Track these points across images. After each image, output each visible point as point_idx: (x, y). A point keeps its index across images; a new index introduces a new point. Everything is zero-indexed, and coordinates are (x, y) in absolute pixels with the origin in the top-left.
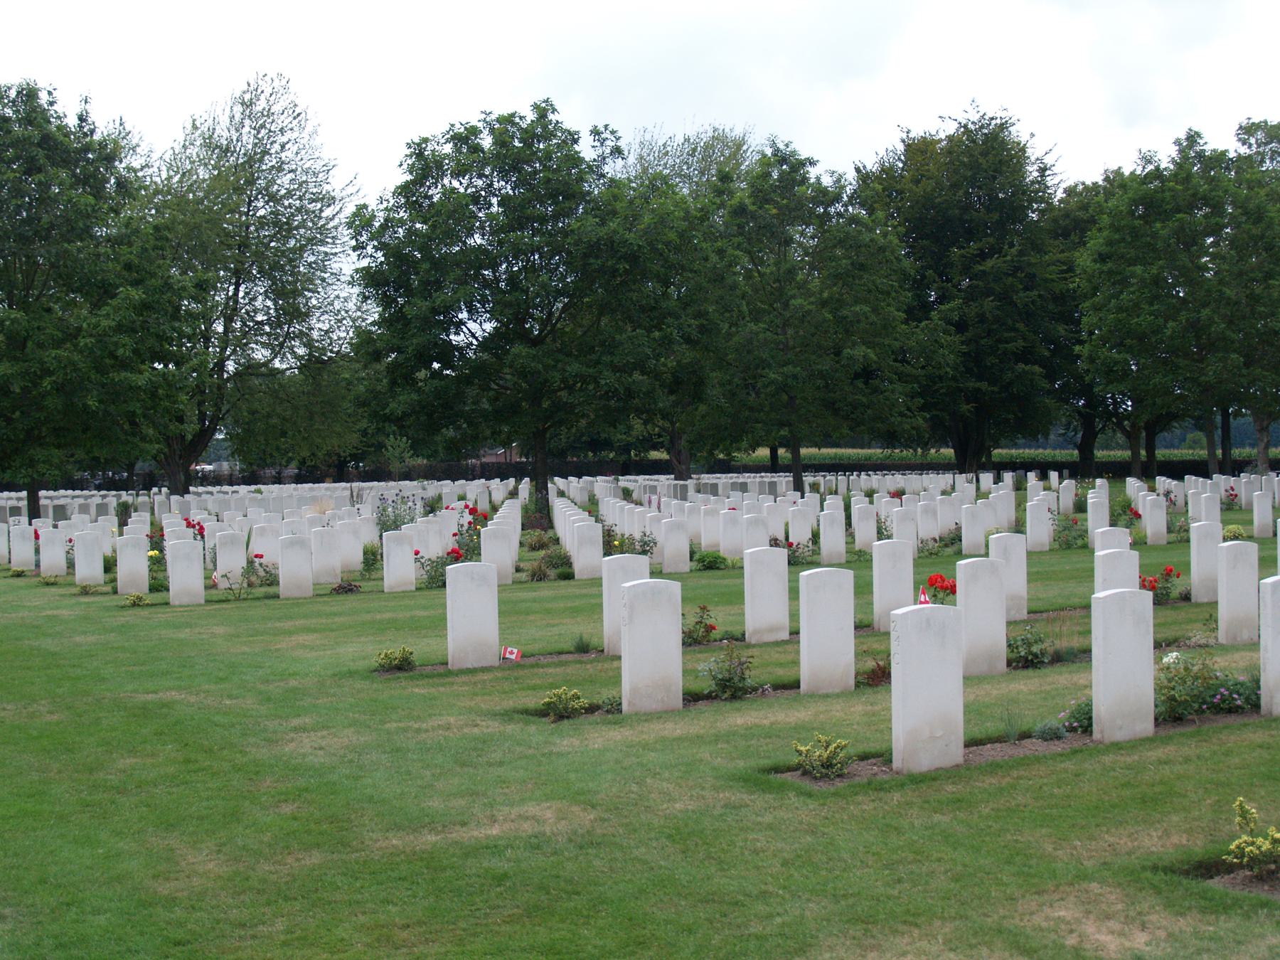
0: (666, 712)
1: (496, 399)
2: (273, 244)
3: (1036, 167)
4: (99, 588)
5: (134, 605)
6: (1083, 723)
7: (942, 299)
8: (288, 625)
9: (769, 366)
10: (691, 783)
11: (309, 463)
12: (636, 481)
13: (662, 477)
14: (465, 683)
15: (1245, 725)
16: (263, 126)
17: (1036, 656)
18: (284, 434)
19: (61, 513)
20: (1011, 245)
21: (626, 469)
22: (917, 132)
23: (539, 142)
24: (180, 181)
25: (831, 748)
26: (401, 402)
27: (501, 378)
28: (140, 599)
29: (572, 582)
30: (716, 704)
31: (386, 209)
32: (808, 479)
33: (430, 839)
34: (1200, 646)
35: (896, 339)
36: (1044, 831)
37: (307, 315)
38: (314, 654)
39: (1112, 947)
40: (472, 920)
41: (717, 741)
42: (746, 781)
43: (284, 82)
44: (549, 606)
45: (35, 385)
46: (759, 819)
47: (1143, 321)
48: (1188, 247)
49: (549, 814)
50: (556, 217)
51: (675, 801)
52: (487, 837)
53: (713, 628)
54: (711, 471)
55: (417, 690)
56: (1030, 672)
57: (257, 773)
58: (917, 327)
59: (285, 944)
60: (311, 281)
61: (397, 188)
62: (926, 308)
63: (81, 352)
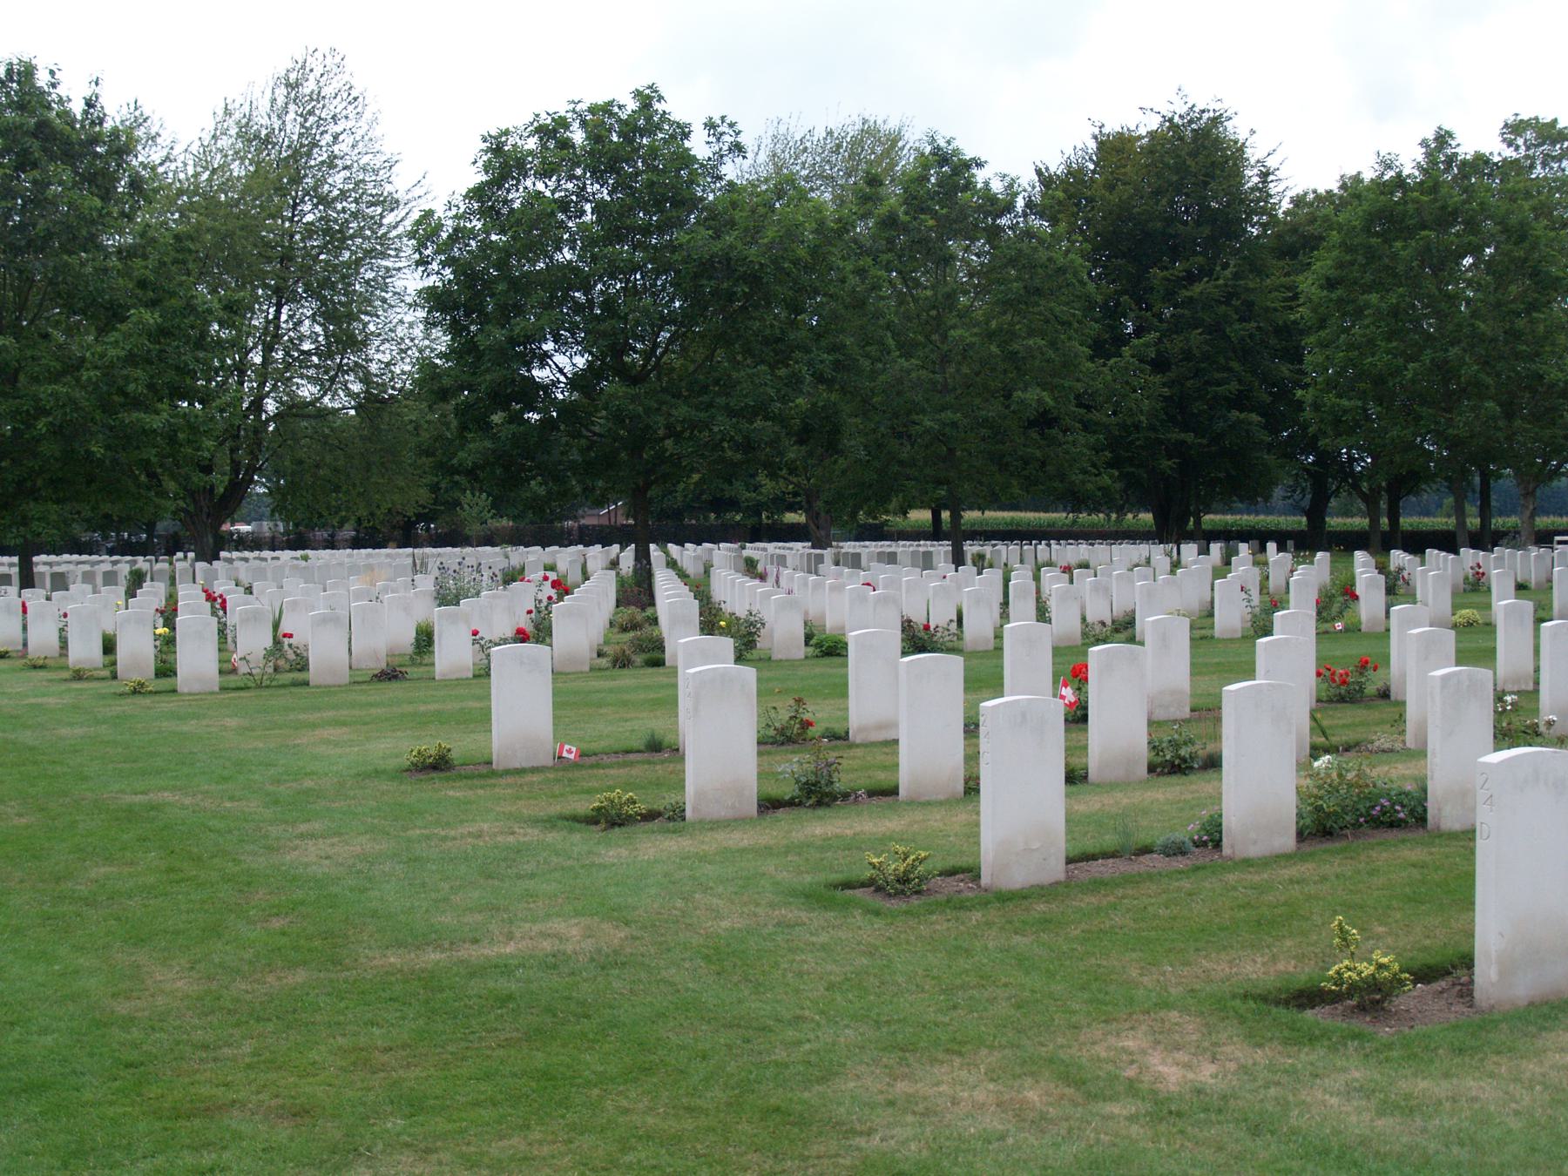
0: (735, 820)
1: (589, 448)
2: (322, 257)
3: (1256, 171)
4: (95, 673)
5: (135, 692)
6: (1212, 838)
7: (1138, 332)
8: (314, 717)
9: (923, 411)
10: (745, 898)
11: (365, 524)
12: (765, 549)
13: (799, 545)
14: (509, 786)
15: (1403, 841)
16: (311, 113)
17: (1184, 760)
18: (337, 489)
19: (60, 582)
20: (1225, 266)
21: (757, 534)
22: (1112, 127)
23: (642, 137)
24: (210, 180)
25: (909, 861)
26: (475, 449)
27: (593, 423)
28: (142, 685)
29: (661, 670)
30: (795, 812)
31: (456, 217)
32: (971, 549)
33: (433, 957)
34: (1384, 751)
35: (1078, 380)
36: (1134, 955)
37: (365, 343)
38: (338, 751)
39: (1173, 1079)
40: (464, 1044)
41: (786, 853)
42: (807, 896)
43: (338, 59)
44: (626, 697)
45: (29, 426)
46: (814, 939)
47: (1378, 361)
48: (1436, 270)
49: (574, 931)
50: (661, 229)
51: (723, 918)
52: (499, 956)
53: (810, 724)
54: (858, 539)
55: (451, 793)
56: (1174, 779)
57: (249, 884)
58: (1105, 365)
59: (249, 1066)
60: (369, 302)
61: (470, 191)
62: (1122, 340)
63: (84, 387)
